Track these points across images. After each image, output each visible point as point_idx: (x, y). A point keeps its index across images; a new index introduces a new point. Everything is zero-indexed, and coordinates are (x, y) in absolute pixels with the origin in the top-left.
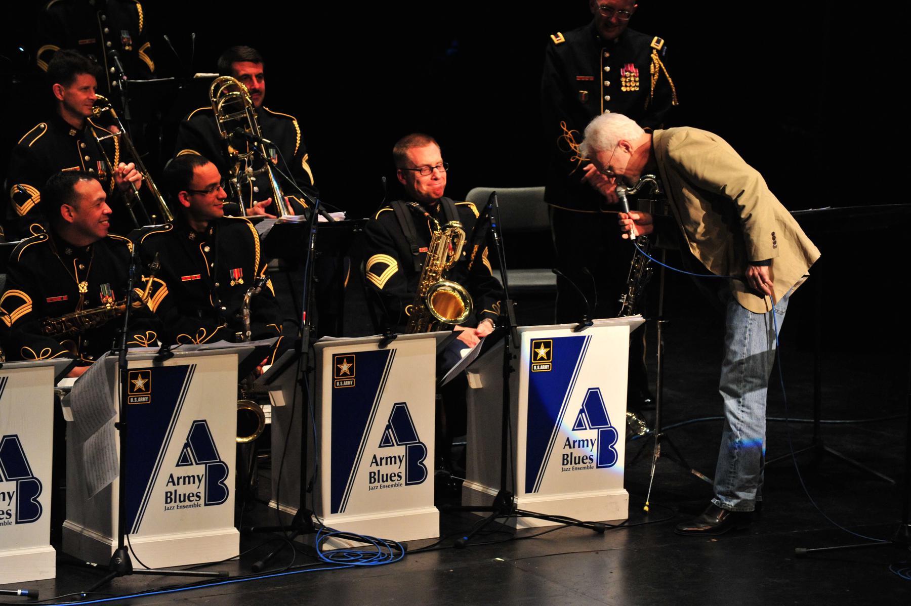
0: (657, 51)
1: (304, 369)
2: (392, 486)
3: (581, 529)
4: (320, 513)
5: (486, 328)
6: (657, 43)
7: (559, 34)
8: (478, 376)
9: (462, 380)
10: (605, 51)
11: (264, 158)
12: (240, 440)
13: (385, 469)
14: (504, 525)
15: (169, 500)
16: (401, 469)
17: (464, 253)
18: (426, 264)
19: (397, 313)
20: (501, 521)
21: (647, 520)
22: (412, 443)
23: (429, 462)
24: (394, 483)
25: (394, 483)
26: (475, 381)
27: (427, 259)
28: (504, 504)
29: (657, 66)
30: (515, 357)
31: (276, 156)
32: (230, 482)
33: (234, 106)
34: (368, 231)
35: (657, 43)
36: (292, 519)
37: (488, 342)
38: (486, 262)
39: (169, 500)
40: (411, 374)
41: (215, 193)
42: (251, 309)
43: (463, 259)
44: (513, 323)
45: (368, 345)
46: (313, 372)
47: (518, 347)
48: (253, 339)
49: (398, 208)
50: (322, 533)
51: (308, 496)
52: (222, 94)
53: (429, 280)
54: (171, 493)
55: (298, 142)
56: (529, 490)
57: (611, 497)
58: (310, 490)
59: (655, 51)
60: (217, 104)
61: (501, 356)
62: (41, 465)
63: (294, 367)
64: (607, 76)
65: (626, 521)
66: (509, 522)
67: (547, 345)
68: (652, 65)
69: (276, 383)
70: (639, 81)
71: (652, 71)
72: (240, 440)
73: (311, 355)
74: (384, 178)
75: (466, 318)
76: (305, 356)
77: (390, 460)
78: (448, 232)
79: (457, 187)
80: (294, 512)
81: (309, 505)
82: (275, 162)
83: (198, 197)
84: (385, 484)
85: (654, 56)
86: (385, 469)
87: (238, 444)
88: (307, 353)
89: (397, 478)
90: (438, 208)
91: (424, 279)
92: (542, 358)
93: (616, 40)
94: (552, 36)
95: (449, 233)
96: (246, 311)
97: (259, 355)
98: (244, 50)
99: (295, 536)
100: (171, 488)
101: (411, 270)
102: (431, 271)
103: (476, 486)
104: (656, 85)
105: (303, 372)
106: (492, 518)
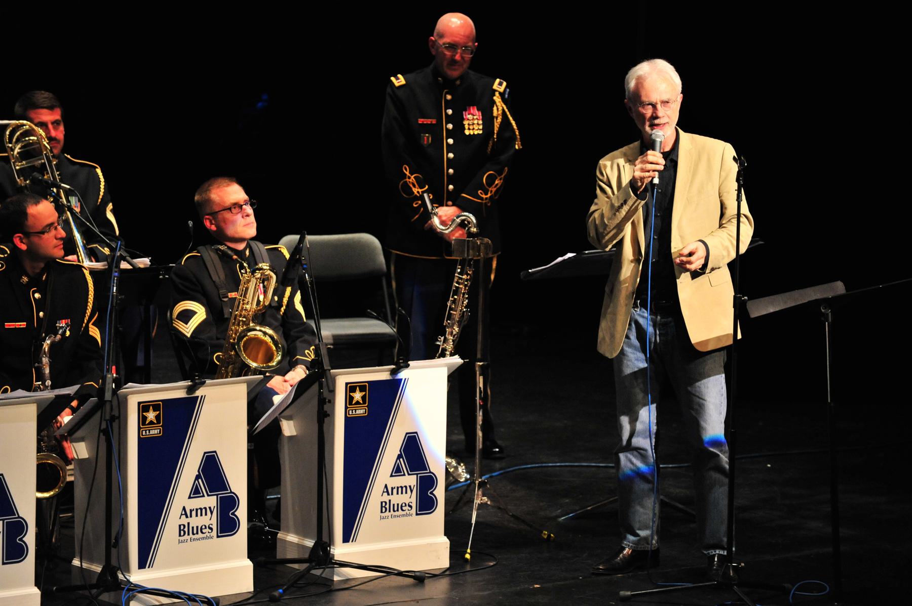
0: (500, 93)
1: (108, 417)
2: (403, 515)
3: (400, 578)
4: (127, 569)
5: (299, 374)
6: (499, 86)
7: (399, 76)
8: (291, 422)
9: (275, 427)
10: (447, 93)
11: (63, 205)
12: (40, 495)
13: (196, 522)
14: (320, 577)
15: (182, 533)
16: (412, 498)
17: (276, 298)
18: (235, 309)
19: (199, 362)
20: (317, 572)
21: (468, 568)
22: (423, 473)
23: (242, 512)
24: (204, 535)
25: (204, 535)
26: (288, 428)
27: (237, 303)
28: (321, 555)
29: (500, 108)
30: (330, 401)
31: (79, 204)
32: (30, 539)
33: (30, 152)
34: (174, 277)
35: (499, 86)
36: (96, 577)
37: (302, 387)
38: (299, 307)
39: (182, 533)
40: (221, 421)
41: (53, 232)
42: (50, 358)
43: (274, 304)
44: (326, 366)
45: (176, 391)
46: (117, 421)
47: (333, 391)
48: (53, 387)
49: (209, 255)
50: (129, 590)
51: (114, 551)
52: (18, 141)
53: (239, 325)
54: (184, 526)
55: (102, 190)
56: (346, 539)
57: (431, 545)
58: (116, 545)
59: (497, 94)
60: (13, 150)
61: (315, 402)
62: (26, 499)
63: (97, 416)
64: (449, 119)
65: (448, 569)
66: (326, 573)
67: (362, 388)
68: (495, 108)
69: (79, 434)
70: (483, 124)
71: (495, 113)
72: (40, 495)
73: (115, 403)
74: (191, 223)
75: (279, 363)
76: (108, 407)
77: (201, 511)
78: (258, 275)
79: (268, 232)
80: (98, 569)
81: (115, 562)
82: (78, 210)
83: (35, 239)
84: (396, 513)
85: (497, 99)
86: (196, 522)
87: (39, 500)
88: (111, 401)
89: (208, 530)
90: (247, 253)
91: (234, 324)
92: (358, 403)
93: (458, 82)
94: (393, 79)
95: (259, 276)
96: (45, 360)
97: (60, 404)
98: (43, 96)
99: (100, 594)
100: (184, 521)
101: (219, 316)
102: (241, 315)
103: (292, 538)
104: (500, 128)
105: (106, 421)
106: (308, 570)
